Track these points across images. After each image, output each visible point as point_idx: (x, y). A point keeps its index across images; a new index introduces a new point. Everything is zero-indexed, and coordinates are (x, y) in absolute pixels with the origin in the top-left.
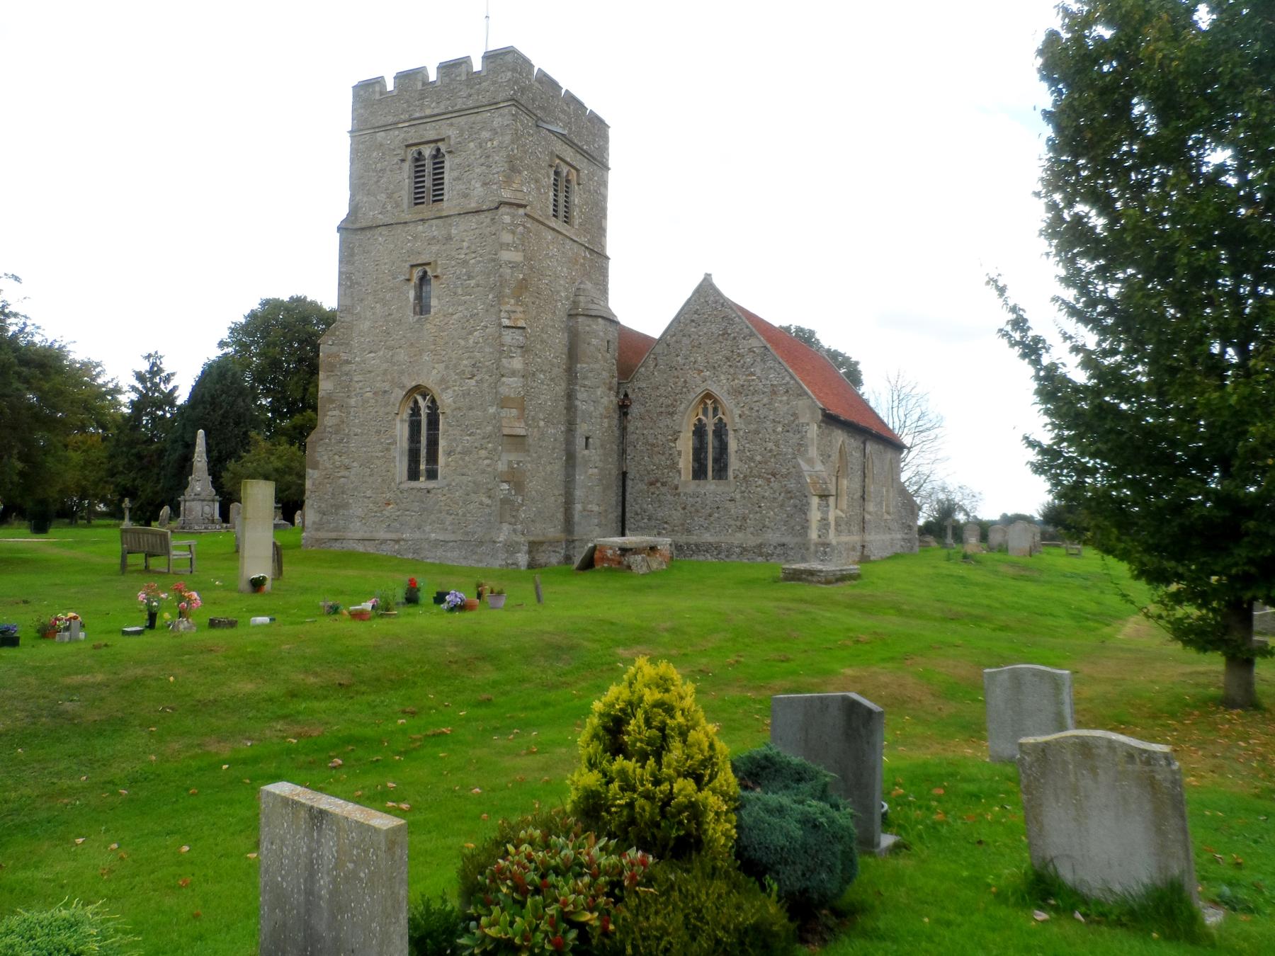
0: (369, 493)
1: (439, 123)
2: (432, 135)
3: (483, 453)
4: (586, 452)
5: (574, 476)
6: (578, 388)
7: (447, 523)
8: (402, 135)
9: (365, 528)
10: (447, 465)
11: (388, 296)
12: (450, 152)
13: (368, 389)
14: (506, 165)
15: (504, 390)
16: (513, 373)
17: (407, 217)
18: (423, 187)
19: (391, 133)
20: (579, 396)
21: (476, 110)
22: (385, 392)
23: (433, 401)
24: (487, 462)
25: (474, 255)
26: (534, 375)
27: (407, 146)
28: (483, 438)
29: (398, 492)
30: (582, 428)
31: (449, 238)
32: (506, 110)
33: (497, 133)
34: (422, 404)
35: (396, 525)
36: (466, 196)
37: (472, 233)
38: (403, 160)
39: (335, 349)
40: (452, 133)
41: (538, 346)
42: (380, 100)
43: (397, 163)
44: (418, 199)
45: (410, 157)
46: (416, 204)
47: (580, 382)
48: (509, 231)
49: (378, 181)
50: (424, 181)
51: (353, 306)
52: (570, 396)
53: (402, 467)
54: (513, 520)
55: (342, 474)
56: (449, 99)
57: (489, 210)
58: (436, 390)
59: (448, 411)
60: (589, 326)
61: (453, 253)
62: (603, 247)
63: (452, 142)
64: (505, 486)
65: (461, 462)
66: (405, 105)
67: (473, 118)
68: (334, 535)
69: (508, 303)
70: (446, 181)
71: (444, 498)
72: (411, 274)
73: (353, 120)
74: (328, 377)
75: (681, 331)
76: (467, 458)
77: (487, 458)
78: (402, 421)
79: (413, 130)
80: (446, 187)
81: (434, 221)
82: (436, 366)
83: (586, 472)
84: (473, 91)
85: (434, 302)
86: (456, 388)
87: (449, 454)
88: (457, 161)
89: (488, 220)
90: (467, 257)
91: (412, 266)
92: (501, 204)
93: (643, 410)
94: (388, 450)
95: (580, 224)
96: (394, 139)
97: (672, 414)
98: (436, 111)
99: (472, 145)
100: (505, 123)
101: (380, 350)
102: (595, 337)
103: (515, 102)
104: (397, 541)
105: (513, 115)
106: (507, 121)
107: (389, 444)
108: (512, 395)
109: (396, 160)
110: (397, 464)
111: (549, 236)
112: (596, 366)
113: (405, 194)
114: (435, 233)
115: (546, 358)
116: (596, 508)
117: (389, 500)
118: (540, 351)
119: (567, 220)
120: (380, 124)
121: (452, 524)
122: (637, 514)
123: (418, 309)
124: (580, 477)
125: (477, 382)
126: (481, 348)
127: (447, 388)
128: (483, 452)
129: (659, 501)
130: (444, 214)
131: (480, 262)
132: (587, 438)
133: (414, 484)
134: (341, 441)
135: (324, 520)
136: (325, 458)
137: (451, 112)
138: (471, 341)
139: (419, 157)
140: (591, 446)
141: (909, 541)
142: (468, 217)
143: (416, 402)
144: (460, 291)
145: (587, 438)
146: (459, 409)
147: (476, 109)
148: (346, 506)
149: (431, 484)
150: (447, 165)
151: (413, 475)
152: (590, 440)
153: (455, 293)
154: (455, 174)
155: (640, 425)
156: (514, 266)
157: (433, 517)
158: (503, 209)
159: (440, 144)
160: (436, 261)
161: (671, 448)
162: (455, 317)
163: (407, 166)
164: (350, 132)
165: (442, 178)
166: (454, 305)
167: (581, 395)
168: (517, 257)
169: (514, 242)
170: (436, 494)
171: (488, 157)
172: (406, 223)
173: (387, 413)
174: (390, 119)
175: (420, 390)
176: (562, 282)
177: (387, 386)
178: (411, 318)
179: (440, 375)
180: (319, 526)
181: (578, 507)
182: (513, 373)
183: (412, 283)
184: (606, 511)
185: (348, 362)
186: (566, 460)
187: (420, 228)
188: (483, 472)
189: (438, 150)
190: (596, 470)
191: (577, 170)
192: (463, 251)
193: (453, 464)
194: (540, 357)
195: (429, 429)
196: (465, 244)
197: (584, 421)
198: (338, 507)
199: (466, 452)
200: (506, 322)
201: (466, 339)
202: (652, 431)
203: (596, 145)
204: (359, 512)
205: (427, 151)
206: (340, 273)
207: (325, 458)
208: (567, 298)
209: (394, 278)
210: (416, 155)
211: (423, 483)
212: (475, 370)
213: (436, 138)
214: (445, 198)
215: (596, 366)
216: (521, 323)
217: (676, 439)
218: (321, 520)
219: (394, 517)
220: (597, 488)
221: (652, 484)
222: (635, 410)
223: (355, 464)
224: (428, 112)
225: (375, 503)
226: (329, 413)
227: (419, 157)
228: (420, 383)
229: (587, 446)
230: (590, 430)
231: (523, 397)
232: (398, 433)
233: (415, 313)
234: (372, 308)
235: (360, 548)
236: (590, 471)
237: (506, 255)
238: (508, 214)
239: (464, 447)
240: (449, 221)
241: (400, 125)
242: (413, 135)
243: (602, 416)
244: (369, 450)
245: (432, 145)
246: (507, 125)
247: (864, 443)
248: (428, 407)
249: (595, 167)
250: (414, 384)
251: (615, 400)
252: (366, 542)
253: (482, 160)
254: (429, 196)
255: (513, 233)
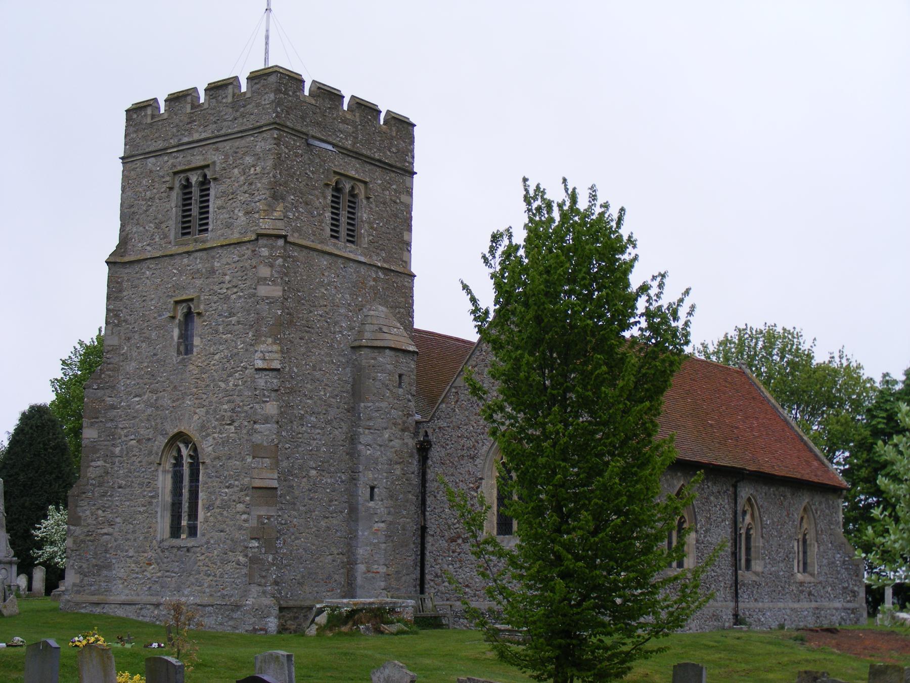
0: (131, 553)
1: (206, 148)
2: (198, 161)
3: (241, 507)
4: (371, 504)
5: (357, 530)
6: (361, 430)
7: (206, 585)
8: (171, 161)
9: (127, 592)
10: (206, 520)
11: (154, 335)
12: (215, 179)
13: (133, 437)
14: (268, 192)
15: (257, 438)
16: (266, 420)
17: (174, 250)
18: (190, 215)
19: (161, 159)
20: (363, 439)
21: (240, 135)
22: (149, 439)
23: (195, 449)
24: (244, 517)
25: (235, 290)
26: (302, 418)
27: (175, 173)
28: (241, 490)
29: (159, 551)
30: (366, 477)
31: (212, 271)
32: (269, 133)
33: (259, 158)
34: (185, 452)
35: (157, 587)
36: (229, 226)
37: (234, 265)
38: (171, 189)
39: (100, 393)
40: (218, 158)
41: (309, 386)
42: (151, 124)
43: (165, 192)
44: (185, 229)
45: (177, 185)
46: (184, 234)
47: (363, 423)
48: (266, 264)
49: (147, 211)
50: (190, 210)
51: (120, 346)
52: (353, 440)
53: (163, 524)
54: (263, 581)
55: (105, 531)
56: (215, 123)
57: (249, 241)
58: (196, 437)
59: (207, 461)
60: (374, 359)
61: (216, 288)
62: (407, 263)
63: (217, 169)
64: (255, 544)
65: (220, 518)
66: (175, 130)
67: (237, 143)
68: (95, 599)
69: (264, 342)
70: (211, 209)
71: (203, 557)
72: (175, 310)
73: (126, 145)
74: (92, 424)
75: (483, 360)
76: (225, 513)
77: (244, 513)
78: (165, 471)
79: (181, 155)
80: (211, 216)
81: (198, 254)
82: (197, 411)
83: (371, 527)
84: (238, 114)
85: (197, 341)
86: (216, 435)
87: (208, 508)
88: (222, 188)
89: (249, 252)
90: (229, 292)
91: (177, 302)
92: (260, 236)
93: (443, 454)
94: (150, 503)
95: (371, 242)
96: (161, 166)
97: (473, 458)
98: (204, 136)
99: (236, 171)
100: (268, 147)
101: (144, 394)
102: (383, 371)
103: (278, 126)
104: (157, 605)
105: (275, 138)
106: (269, 145)
107: (152, 497)
108: (265, 444)
109: (164, 187)
110: (159, 520)
111: (324, 262)
112: (384, 405)
113: (172, 225)
114: (200, 266)
115: (321, 399)
116: (383, 569)
117: (150, 559)
118: (311, 391)
119: (352, 238)
120: (151, 149)
121: (209, 586)
122: (437, 576)
123: (182, 348)
124: (363, 533)
125: (236, 428)
126: (240, 391)
127: (208, 435)
128: (241, 505)
129: (460, 561)
130: (208, 245)
131: (240, 297)
132: (372, 488)
133: (175, 542)
134: (104, 495)
135: (85, 582)
136: (88, 513)
137: (217, 137)
138: (231, 384)
139: (187, 185)
140: (376, 498)
141: (853, 611)
142: (231, 248)
143: (179, 451)
144: (221, 329)
145: (372, 488)
146: (218, 458)
147: (242, 134)
148: (109, 567)
149: (191, 542)
150: (212, 192)
151: (175, 531)
152: (376, 490)
153: (217, 331)
154: (219, 202)
155: (440, 471)
156: (271, 301)
157: (192, 579)
158: (261, 242)
159: (206, 171)
160: (199, 297)
161: (472, 498)
162: (217, 357)
163: (176, 195)
164: (122, 158)
165: (208, 206)
166: (215, 344)
167: (365, 437)
168: (276, 291)
169: (272, 275)
170: (195, 553)
171: (251, 184)
172: (171, 255)
173: (151, 463)
174: (161, 144)
175: (181, 437)
176: (342, 311)
177: (150, 433)
178: (174, 358)
179: (200, 421)
180: (79, 588)
181: (361, 568)
182: (266, 420)
183: (177, 321)
184: (397, 572)
185: (113, 407)
186: (349, 513)
187: (186, 261)
188: (240, 528)
189: (205, 176)
190: (382, 525)
191: (365, 183)
192: (225, 286)
193: (211, 519)
194: (311, 398)
195: (191, 481)
196: (227, 278)
197: (367, 468)
198: (100, 568)
199: (225, 506)
200: (260, 364)
201: (226, 381)
202: (452, 478)
203: (394, 150)
204: (122, 573)
205: (194, 178)
206: (108, 310)
207: (88, 513)
208: (351, 328)
209: (160, 316)
210: (184, 182)
211: (184, 540)
212: (234, 415)
213: (202, 163)
214: (210, 227)
215: (384, 405)
216: (276, 365)
217: (478, 488)
218: (82, 581)
219: (154, 579)
220: (383, 546)
221: (453, 540)
222: (436, 453)
223: (118, 520)
224: (196, 136)
225: (136, 563)
226: (93, 464)
227: (187, 185)
228: (182, 429)
229: (372, 498)
230: (375, 479)
231: (277, 446)
232: (160, 485)
233: (179, 353)
234: (138, 348)
235: (120, 612)
236: (376, 526)
237: (263, 291)
238: (265, 246)
239: (223, 500)
240: (213, 253)
241: (169, 151)
242: (181, 162)
243: (390, 462)
244: (132, 504)
245: (199, 172)
246: (269, 150)
247: (735, 486)
248: (191, 457)
249: (393, 175)
250: (176, 431)
251: (411, 443)
252: (128, 607)
253: (246, 187)
254: (195, 226)
255: (271, 266)
